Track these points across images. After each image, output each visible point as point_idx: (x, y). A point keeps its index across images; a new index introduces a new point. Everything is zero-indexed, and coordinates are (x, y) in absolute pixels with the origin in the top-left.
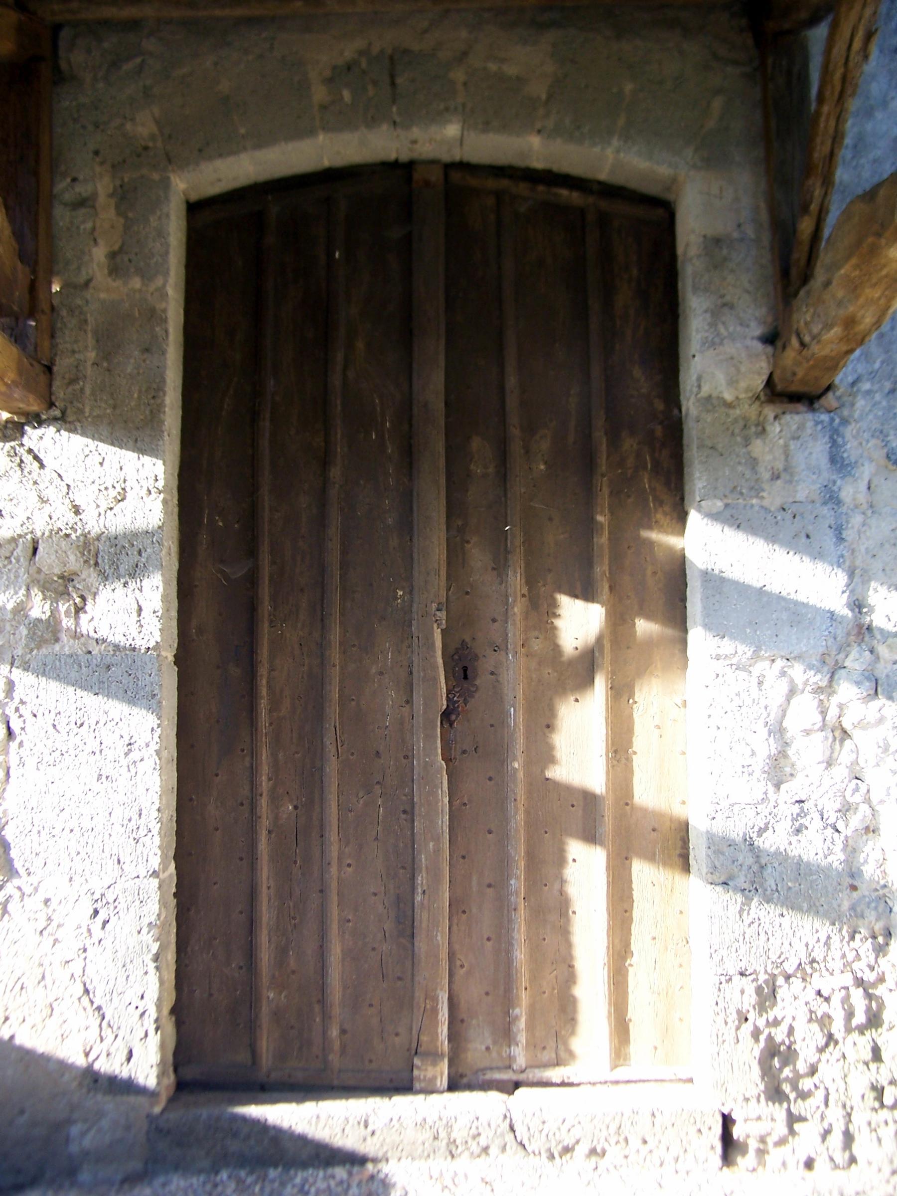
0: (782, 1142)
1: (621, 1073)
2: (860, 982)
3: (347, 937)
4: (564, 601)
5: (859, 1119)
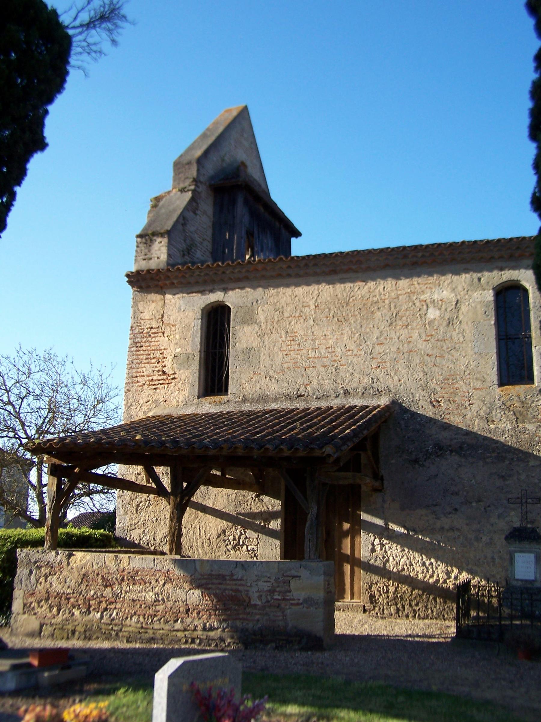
0: (373, 610)
1: (352, 601)
2: (385, 585)
3: (231, 592)
4: (344, 523)
5: (385, 607)
